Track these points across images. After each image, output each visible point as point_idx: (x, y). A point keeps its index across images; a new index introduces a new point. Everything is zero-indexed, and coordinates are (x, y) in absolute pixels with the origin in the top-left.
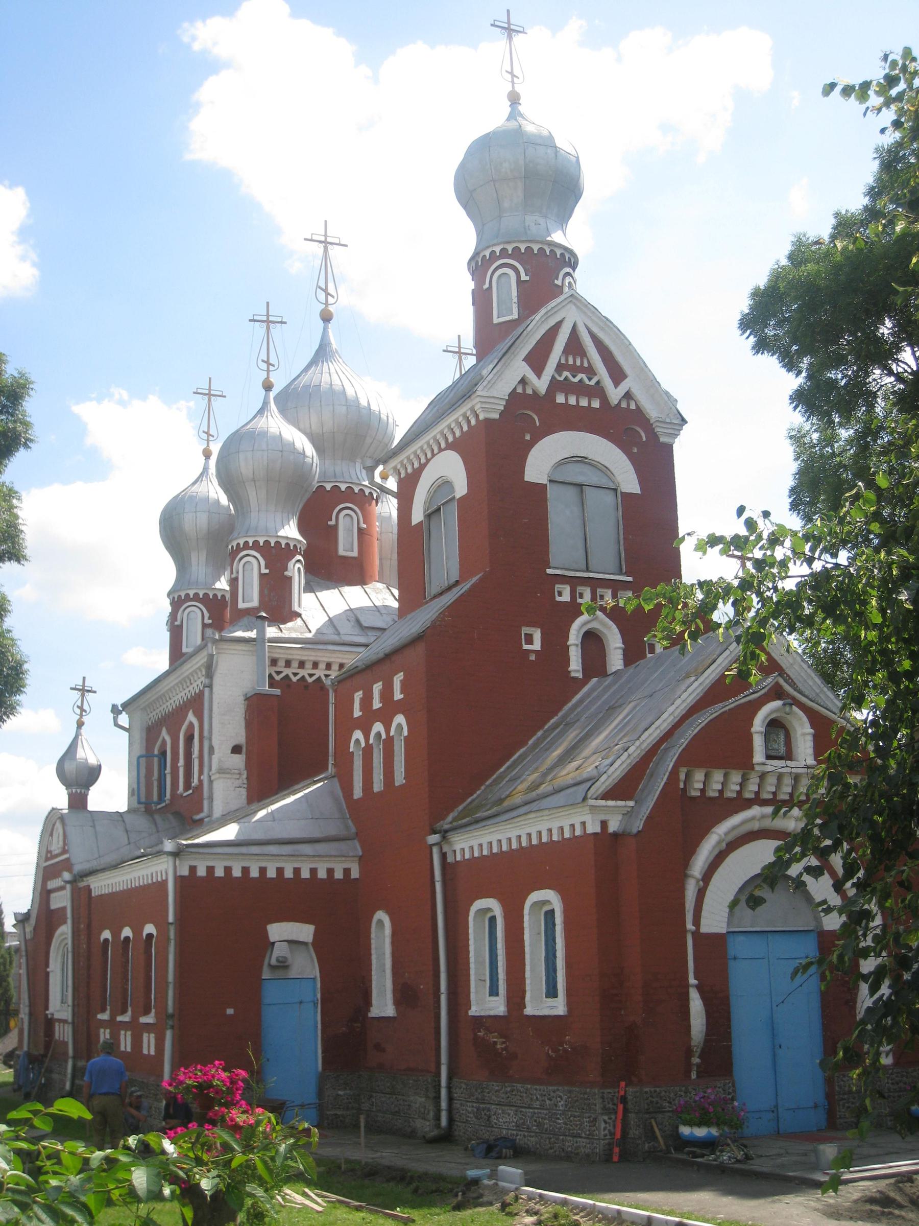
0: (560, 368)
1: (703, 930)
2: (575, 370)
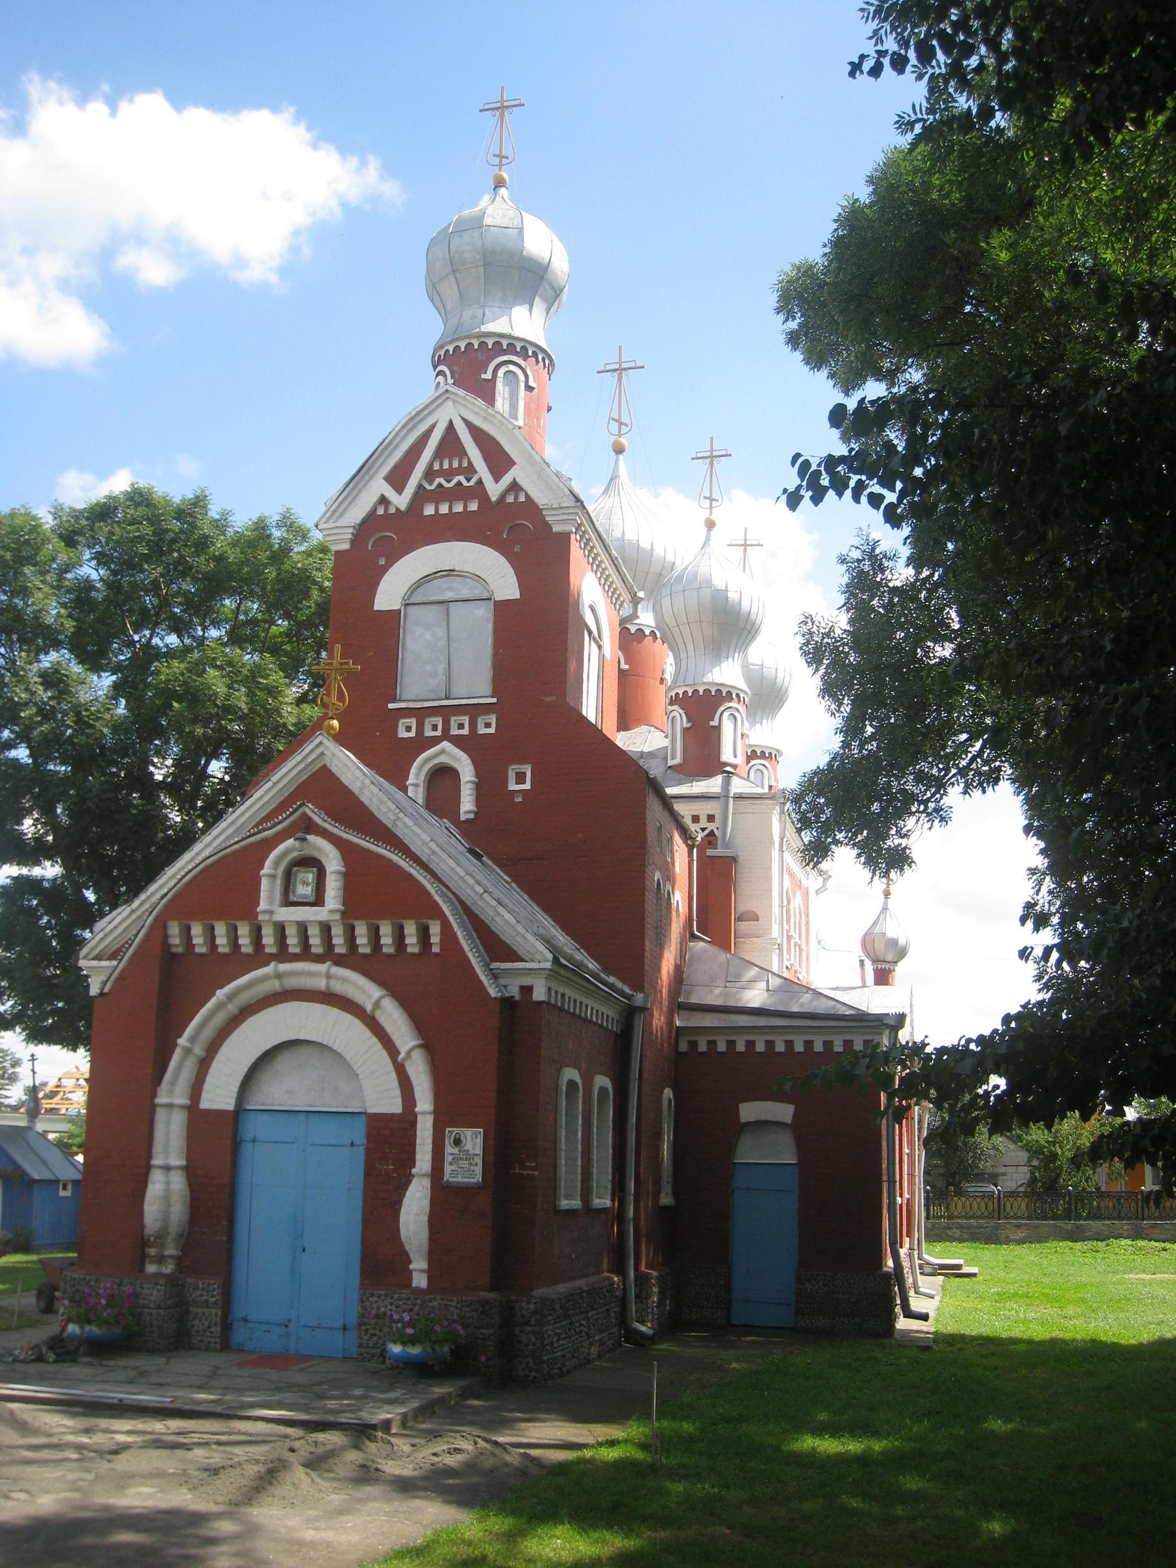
0: (429, 474)
1: (205, 1104)
2: (449, 474)
